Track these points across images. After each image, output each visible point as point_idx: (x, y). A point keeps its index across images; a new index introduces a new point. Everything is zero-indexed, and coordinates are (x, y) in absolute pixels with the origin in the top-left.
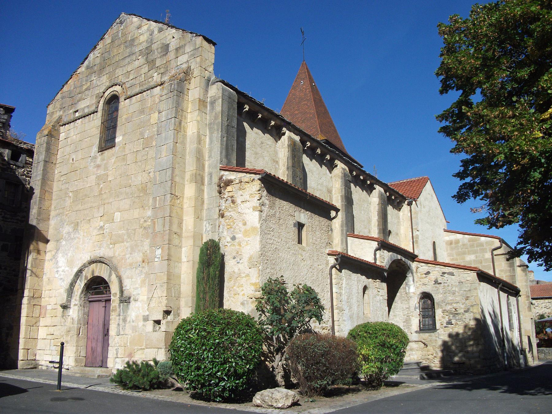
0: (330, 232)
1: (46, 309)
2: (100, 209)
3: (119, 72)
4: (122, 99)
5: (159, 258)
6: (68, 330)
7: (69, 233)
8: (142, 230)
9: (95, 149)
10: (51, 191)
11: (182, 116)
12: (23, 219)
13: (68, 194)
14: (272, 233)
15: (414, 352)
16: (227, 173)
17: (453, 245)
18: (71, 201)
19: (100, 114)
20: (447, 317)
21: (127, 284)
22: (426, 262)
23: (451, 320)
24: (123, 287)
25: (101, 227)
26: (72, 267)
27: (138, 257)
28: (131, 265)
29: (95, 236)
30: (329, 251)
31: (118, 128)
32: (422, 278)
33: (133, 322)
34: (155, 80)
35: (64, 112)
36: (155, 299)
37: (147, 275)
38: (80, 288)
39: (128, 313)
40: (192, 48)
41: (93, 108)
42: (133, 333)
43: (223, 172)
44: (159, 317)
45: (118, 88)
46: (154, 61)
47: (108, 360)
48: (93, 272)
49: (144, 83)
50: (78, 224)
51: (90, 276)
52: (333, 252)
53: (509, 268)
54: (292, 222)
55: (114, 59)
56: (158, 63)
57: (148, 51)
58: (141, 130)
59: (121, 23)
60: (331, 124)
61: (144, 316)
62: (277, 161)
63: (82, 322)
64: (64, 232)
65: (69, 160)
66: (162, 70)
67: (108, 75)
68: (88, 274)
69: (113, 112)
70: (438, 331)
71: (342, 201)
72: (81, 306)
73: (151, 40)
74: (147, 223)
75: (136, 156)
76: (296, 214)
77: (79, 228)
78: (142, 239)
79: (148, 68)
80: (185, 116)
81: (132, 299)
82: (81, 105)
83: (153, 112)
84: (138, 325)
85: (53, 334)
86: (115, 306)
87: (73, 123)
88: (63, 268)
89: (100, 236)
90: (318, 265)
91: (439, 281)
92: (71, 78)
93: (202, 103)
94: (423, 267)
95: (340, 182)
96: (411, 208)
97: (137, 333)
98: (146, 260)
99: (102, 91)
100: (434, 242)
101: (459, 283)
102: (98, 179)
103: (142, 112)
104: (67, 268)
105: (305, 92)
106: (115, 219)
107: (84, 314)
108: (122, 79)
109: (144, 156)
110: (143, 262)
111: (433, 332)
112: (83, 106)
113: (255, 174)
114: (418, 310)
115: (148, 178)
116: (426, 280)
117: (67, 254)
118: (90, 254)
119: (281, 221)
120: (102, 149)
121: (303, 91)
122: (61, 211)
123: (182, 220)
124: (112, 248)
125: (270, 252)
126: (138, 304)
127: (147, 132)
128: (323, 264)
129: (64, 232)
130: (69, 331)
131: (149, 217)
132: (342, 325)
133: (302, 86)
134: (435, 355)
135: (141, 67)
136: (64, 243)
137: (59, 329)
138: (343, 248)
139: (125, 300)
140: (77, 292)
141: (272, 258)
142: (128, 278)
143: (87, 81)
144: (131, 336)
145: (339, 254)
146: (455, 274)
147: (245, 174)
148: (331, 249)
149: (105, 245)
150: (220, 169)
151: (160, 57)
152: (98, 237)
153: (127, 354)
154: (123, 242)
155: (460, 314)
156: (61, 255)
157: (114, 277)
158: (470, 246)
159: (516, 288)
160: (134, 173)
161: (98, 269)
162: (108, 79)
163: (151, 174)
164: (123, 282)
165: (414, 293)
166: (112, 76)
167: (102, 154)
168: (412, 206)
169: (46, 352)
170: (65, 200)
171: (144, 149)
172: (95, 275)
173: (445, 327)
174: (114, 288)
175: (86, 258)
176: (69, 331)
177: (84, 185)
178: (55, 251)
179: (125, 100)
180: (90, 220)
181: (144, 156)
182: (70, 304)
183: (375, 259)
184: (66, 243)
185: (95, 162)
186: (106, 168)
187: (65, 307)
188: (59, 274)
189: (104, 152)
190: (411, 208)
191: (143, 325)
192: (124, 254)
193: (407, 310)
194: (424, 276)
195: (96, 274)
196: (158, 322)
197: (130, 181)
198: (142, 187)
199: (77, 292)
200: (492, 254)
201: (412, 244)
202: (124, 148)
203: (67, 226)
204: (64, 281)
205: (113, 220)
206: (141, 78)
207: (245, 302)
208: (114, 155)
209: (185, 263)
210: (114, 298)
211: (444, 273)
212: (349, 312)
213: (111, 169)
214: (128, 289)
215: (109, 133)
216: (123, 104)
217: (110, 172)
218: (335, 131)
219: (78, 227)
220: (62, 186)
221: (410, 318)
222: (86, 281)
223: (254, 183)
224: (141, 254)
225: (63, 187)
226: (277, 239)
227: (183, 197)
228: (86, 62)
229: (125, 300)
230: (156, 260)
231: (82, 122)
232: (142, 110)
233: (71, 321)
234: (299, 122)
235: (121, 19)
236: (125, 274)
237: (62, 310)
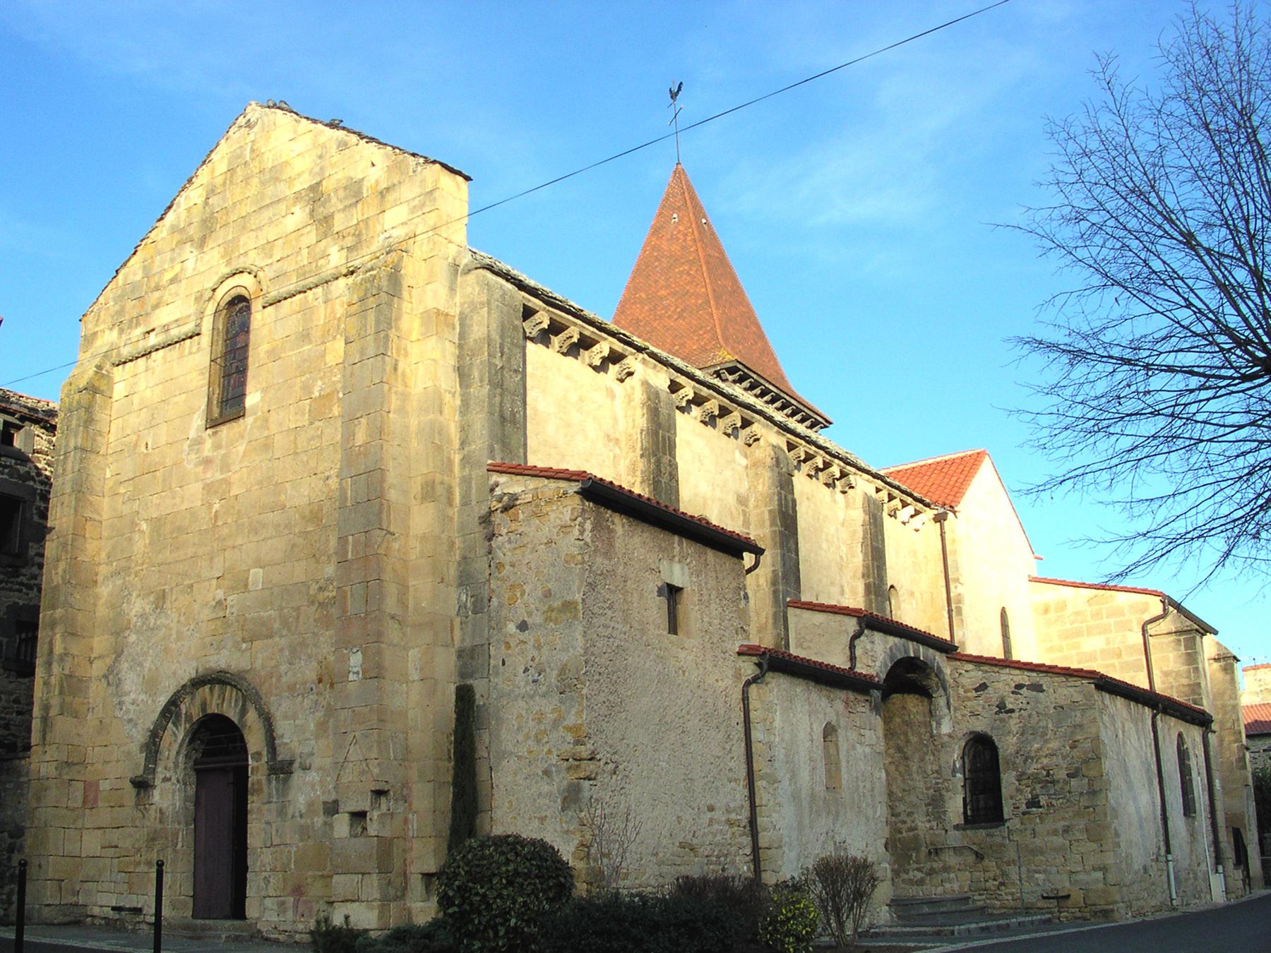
0: (743, 602)
1: (97, 790)
2: (216, 560)
3: (249, 241)
4: (256, 306)
5: (357, 673)
6: (151, 835)
7: (143, 616)
8: (313, 608)
9: (198, 420)
10: (98, 518)
11: (398, 350)
12: (33, 582)
13: (137, 525)
14: (609, 613)
15: (952, 875)
16: (503, 479)
17: (1052, 615)
18: (147, 542)
19: (205, 339)
20: (1029, 789)
21: (283, 728)
22: (979, 661)
23: (1037, 796)
24: (274, 739)
25: (219, 603)
27: (309, 672)
28: (291, 688)
30: (742, 646)
31: (250, 373)
32: (969, 699)
33: (301, 816)
34: (332, 265)
35: (121, 331)
36: (351, 765)
37: (330, 711)
38: (175, 741)
39: (290, 797)
40: (417, 191)
41: (188, 328)
42: (302, 840)
43: (495, 478)
44: (363, 804)
45: (246, 280)
46: (328, 219)
47: (248, 902)
48: (204, 705)
49: (307, 269)
50: (164, 596)
51: (196, 714)
52: (750, 647)
53: (1185, 668)
54: (652, 585)
55: (236, 211)
56: (339, 223)
57: (315, 195)
58: (303, 379)
59: (249, 125)
60: (749, 319)
61: (325, 803)
62: (617, 440)
63: (182, 819)
64: (133, 613)
65: (136, 445)
66: (349, 241)
67: (222, 249)
68: (191, 708)
69: (236, 336)
70: (1007, 824)
71: (773, 524)
72: (178, 781)
73: (322, 169)
74: (326, 594)
75: (296, 438)
76: (664, 566)
77: (168, 605)
78: (316, 630)
79: (317, 235)
80: (405, 349)
81: (296, 765)
82: (162, 317)
83: (330, 338)
84: (313, 823)
85: (117, 847)
86: (259, 782)
87: (144, 358)
88: (133, 696)
89: (219, 622)
90: (717, 681)
91: (1009, 706)
92: (134, 254)
93: (442, 318)
94: (972, 674)
95: (767, 478)
96: (942, 528)
97: (311, 842)
98: (326, 678)
99: (211, 285)
100: (1003, 610)
101: (1055, 708)
102: (208, 492)
103: (305, 336)
104: (143, 697)
105: (685, 240)
106: (250, 584)
107: (185, 801)
108: (254, 259)
109: (312, 439)
110: (320, 681)
111: (997, 827)
112: (164, 321)
113: (568, 480)
114: (959, 775)
115: (325, 489)
116: (977, 705)
117: (141, 665)
118: (195, 664)
119: (629, 582)
120: (213, 423)
121: (678, 239)
122: (123, 563)
123: (408, 587)
124: (246, 650)
125: (607, 655)
126: (313, 776)
127: (319, 383)
128: (727, 677)
129: (133, 613)
130: (153, 839)
131: (330, 580)
132: (774, 815)
133: (676, 227)
134: (1001, 880)
135: (301, 232)
136: (133, 638)
137: (131, 835)
138: (778, 635)
139: (282, 769)
140: (169, 751)
141: (610, 669)
142: (286, 717)
143: (172, 260)
144: (297, 847)
145: (764, 653)
146: (1044, 687)
147: (546, 481)
148: (746, 643)
149: (230, 644)
150: (488, 470)
151: (344, 210)
153: (289, 889)
154: (271, 637)
155: (1058, 781)
156: (126, 665)
157: (252, 716)
158: (1093, 616)
159: (1203, 713)
160: (291, 477)
161: (216, 696)
162: (223, 257)
163: (330, 481)
165: (950, 736)
166: (233, 251)
167: (216, 433)
168: (946, 523)
169: (105, 886)
170: (130, 539)
171: (311, 423)
172: (209, 711)
173: (1024, 814)
174: (255, 741)
175: (187, 672)
176: (153, 839)
177: (175, 505)
178: (114, 656)
179: (264, 307)
180: (191, 586)
181: (312, 439)
182: (154, 779)
183: (853, 658)
185: (198, 451)
186: (225, 467)
187: (142, 785)
189: (218, 429)
190: (942, 528)
191: (325, 823)
192: (274, 663)
193: (935, 775)
194: (974, 694)
195: (212, 709)
196: (359, 816)
197: (283, 497)
198: (311, 512)
199: (169, 751)
200: (1144, 631)
201: (947, 616)
202: (267, 420)
203: (139, 601)
205: (246, 586)
206: (299, 258)
207: (554, 769)
208: (242, 437)
209: (415, 683)
210: (255, 764)
211: (1019, 686)
212: (790, 785)
213: (238, 468)
214: (286, 744)
215: (229, 383)
216: (260, 318)
217: (236, 476)
218: (761, 336)
219: (164, 603)
220: (124, 507)
221: (941, 795)
223: (566, 501)
224: (315, 664)
225: (126, 509)
226: (620, 626)
227: (407, 535)
228: (170, 217)
229: (282, 769)
230: (352, 677)
231: (164, 357)
232: (305, 332)
233: (158, 815)
234: (670, 317)
235: (247, 118)
236: (280, 708)
237: (133, 791)
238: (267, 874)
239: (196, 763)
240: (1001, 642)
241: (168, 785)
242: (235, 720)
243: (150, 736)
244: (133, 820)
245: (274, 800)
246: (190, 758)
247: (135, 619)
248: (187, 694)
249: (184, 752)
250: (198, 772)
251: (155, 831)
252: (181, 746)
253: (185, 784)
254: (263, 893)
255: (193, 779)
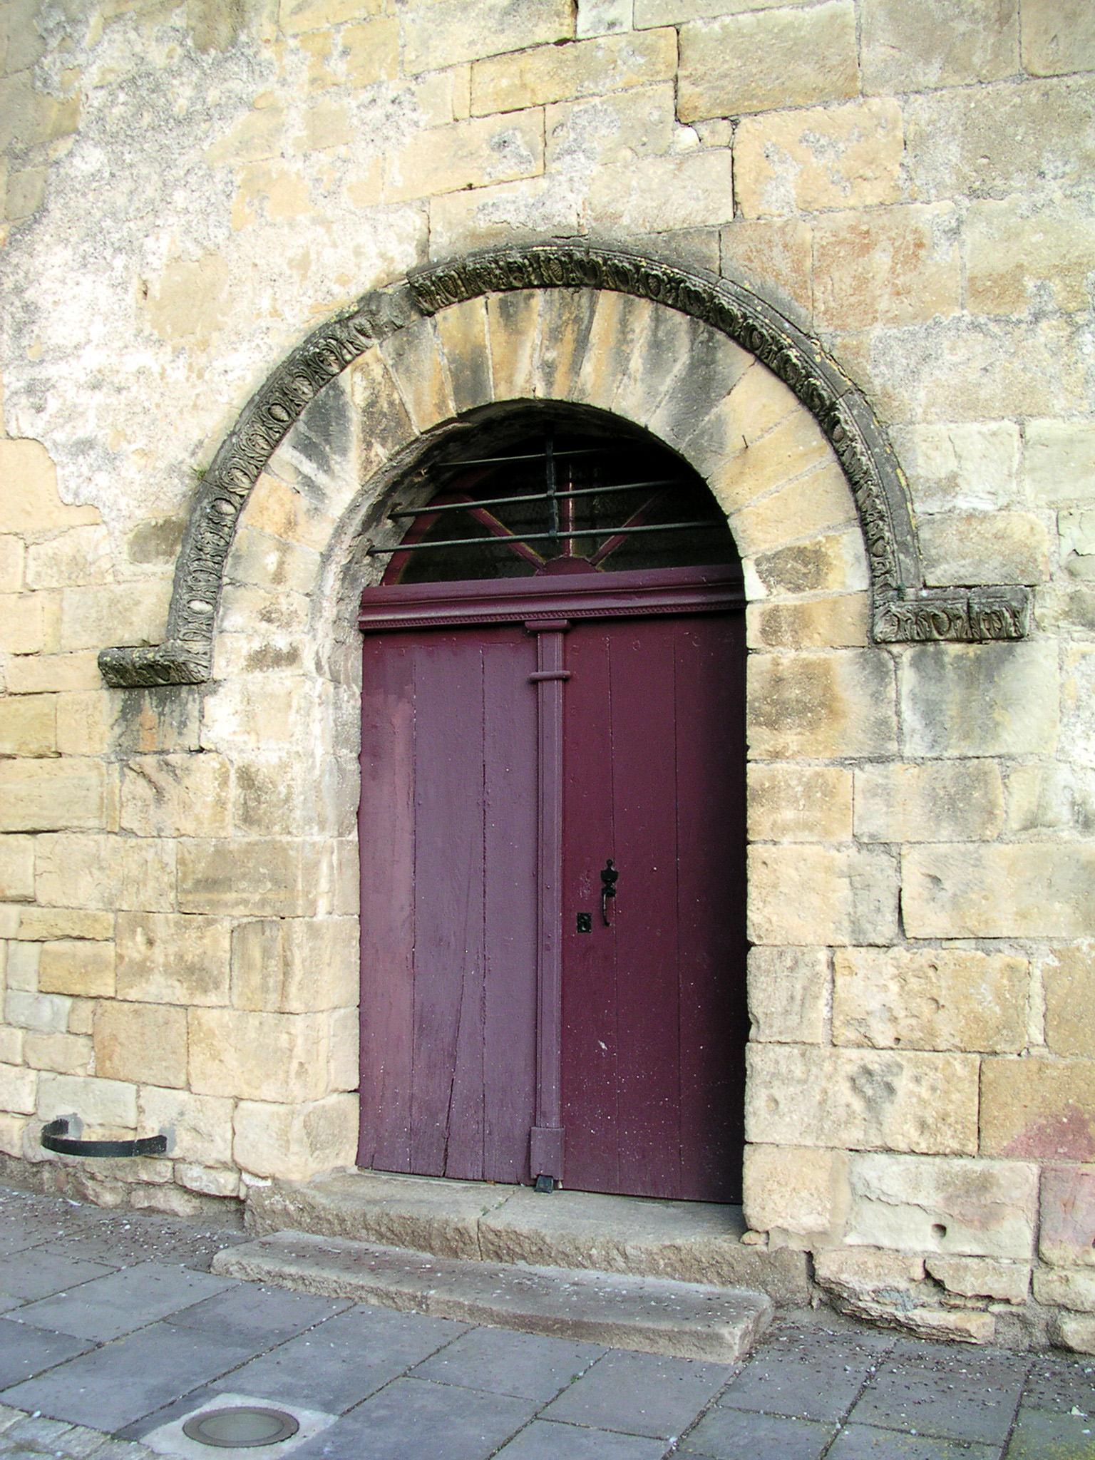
26: (204, 345)
29: (821, 1151)
64: (93, 75)
72: (319, 667)
86: (812, 674)
88: (93, 359)
89: (537, 64)
104: (145, 357)
118: (413, 222)
129: (93, 75)
130: (210, 884)
137: (96, 862)
140: (284, 548)
152: (497, 79)
156: (62, 255)
164: (696, 283)
172: (500, 391)
176: (210, 884)
184: (118, 160)
188: (53, 404)
199: (284, 548)
204: (111, 459)
210: (785, 598)
222: (381, 452)
233: (234, 792)
237: (108, 703)
238: (872, 1059)
239: (368, 604)
240: (790, 401)
241: (282, 678)
242: (657, 422)
243: (198, 496)
244: (107, 806)
245: (915, 746)
246: (354, 579)
247: (98, 98)
248: (378, 331)
249: (341, 558)
250: (370, 633)
251: (221, 853)
252: (339, 531)
253: (336, 680)
254: (854, 1135)
255: (354, 663)
